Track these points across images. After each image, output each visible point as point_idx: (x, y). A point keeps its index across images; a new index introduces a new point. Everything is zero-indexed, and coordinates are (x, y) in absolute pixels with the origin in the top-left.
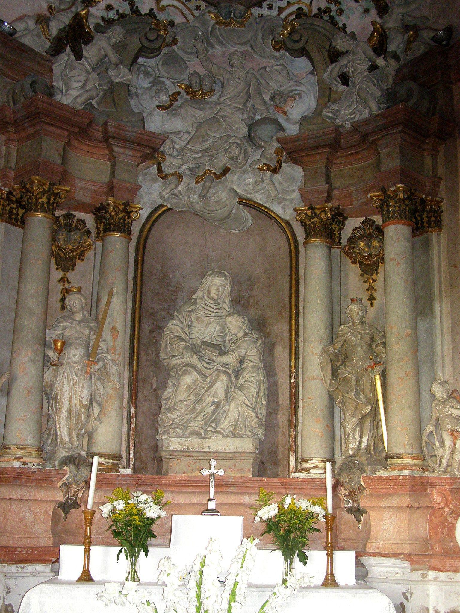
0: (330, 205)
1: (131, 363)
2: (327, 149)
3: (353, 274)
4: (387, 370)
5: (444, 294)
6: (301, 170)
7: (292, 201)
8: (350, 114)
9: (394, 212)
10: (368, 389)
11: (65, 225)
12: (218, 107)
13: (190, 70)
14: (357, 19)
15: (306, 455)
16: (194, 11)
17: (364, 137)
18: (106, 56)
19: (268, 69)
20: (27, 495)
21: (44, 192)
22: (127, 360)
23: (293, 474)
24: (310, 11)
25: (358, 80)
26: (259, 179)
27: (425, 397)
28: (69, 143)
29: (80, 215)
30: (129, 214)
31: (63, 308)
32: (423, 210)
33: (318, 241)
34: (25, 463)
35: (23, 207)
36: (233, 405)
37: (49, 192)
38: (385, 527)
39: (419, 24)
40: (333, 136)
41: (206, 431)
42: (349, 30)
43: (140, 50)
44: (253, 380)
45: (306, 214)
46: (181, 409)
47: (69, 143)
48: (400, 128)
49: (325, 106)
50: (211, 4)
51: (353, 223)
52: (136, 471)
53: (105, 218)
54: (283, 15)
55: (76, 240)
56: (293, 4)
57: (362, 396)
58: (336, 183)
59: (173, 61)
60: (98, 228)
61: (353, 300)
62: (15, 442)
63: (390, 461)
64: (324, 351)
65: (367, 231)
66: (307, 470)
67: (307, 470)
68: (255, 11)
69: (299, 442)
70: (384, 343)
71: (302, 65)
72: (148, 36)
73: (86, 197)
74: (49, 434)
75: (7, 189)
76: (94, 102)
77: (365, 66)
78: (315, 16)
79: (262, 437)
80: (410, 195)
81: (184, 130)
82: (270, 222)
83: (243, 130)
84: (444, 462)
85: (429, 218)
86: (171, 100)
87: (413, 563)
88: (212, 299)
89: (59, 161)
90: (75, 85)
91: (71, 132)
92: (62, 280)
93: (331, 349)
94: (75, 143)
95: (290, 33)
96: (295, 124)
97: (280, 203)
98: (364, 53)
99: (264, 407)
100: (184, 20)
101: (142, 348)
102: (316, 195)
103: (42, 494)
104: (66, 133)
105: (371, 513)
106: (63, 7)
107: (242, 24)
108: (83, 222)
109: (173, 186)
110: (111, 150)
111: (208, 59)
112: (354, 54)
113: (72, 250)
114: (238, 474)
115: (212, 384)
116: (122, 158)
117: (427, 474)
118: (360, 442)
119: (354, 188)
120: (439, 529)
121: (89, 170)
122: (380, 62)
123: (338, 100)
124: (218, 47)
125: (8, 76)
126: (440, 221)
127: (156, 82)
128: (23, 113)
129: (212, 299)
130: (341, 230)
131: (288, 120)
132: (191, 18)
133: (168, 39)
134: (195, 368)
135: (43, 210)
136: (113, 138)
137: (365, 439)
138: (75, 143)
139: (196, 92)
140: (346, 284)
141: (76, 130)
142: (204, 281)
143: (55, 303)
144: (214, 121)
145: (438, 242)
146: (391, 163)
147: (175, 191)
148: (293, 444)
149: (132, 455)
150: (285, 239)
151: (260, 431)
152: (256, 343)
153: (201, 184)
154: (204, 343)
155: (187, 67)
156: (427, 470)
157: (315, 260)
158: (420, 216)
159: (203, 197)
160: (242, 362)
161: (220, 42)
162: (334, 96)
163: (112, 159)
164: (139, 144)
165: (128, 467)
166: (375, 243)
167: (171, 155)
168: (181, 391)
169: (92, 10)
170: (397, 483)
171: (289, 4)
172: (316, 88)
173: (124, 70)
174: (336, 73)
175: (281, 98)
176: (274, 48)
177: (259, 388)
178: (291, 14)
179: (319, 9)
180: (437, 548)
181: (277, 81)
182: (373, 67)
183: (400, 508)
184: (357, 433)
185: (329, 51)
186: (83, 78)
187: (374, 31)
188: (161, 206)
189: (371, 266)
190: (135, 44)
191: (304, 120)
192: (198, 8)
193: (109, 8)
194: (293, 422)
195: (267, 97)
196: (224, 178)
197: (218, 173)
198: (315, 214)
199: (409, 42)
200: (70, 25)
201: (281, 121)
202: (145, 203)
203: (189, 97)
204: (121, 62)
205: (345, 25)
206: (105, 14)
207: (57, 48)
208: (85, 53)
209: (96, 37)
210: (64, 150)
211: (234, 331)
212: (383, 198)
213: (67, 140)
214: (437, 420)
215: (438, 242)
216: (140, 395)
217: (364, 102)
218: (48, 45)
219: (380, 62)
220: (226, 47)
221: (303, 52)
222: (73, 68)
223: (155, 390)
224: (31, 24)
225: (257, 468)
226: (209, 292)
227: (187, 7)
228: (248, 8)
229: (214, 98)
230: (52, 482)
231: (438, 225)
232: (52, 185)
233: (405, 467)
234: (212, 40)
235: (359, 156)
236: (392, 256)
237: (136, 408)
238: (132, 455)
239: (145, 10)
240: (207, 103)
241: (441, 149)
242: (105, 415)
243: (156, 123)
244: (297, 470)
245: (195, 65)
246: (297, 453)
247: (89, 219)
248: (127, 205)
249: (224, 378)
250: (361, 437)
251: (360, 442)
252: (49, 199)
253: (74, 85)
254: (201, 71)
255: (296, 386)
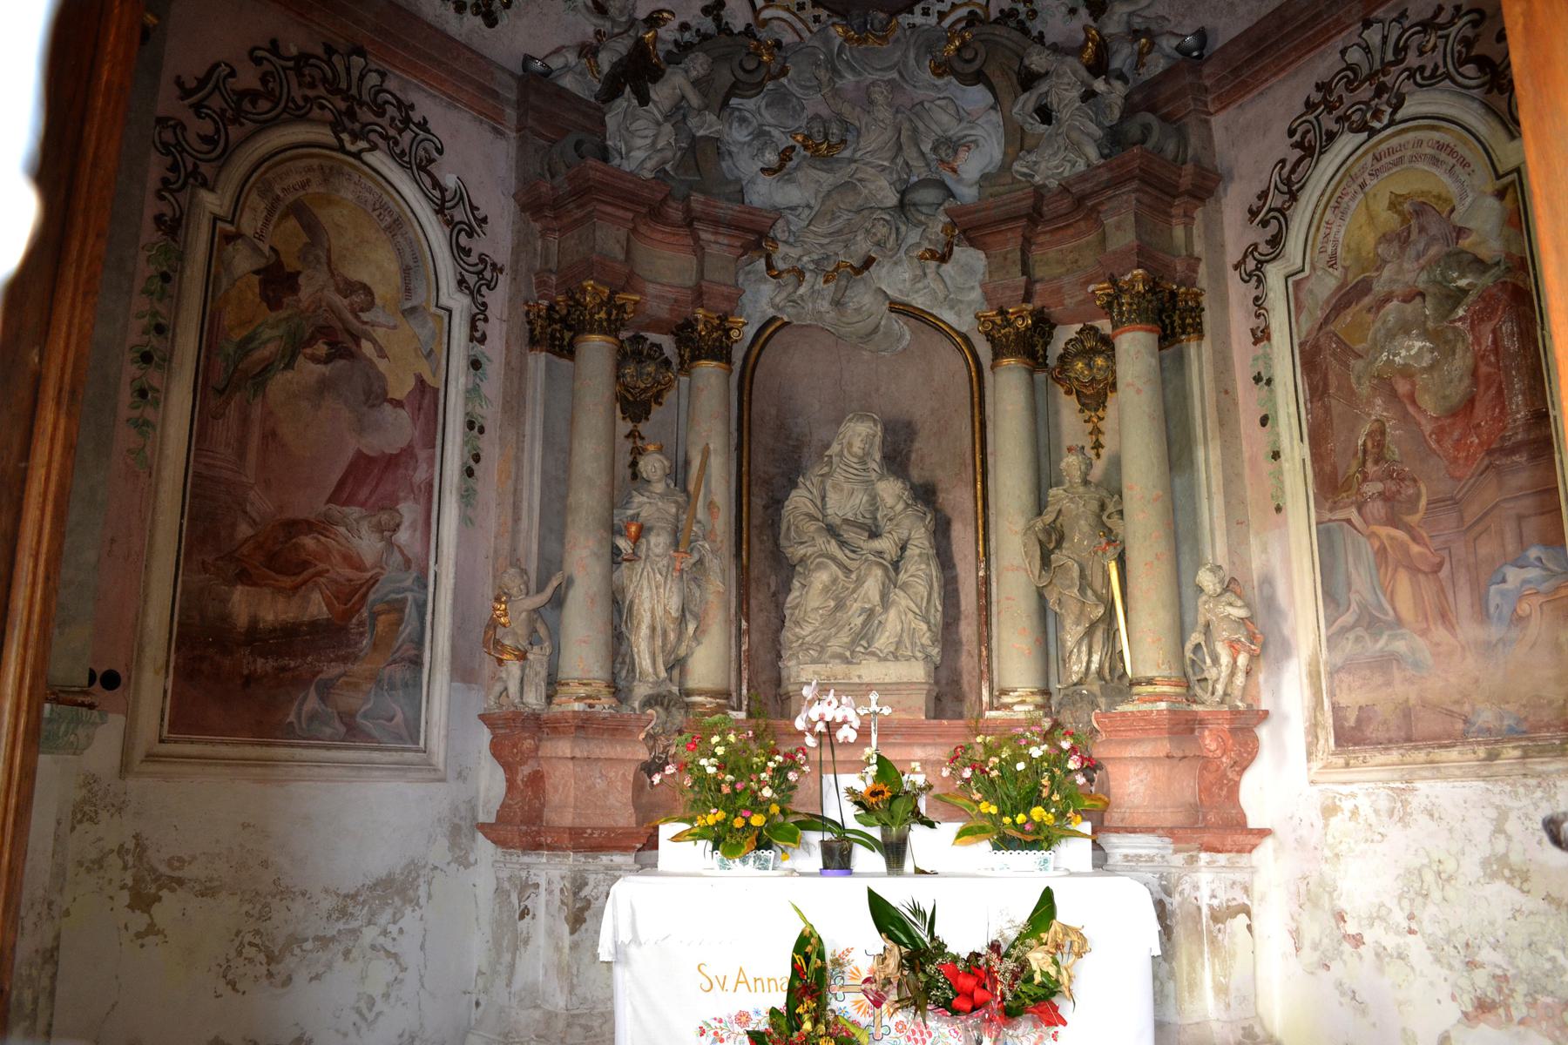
0: (1030, 307)
1: (738, 555)
2: (1023, 222)
3: (1068, 410)
4: (1127, 552)
5: (1209, 434)
6: (983, 256)
7: (970, 304)
8: (1057, 167)
9: (1130, 312)
10: (1098, 583)
11: (632, 353)
12: (854, 166)
13: (809, 112)
14: (1059, 19)
15: (1006, 685)
16: (811, 25)
17: (1080, 201)
18: (683, 97)
19: (927, 105)
20: (597, 753)
21: (601, 304)
22: (733, 550)
23: (988, 714)
24: (987, 14)
25: (1065, 115)
26: (919, 272)
27: (1188, 592)
28: (634, 230)
29: (653, 337)
30: (727, 332)
31: (635, 476)
32: (1174, 308)
33: (1012, 361)
34: (591, 706)
35: (570, 328)
36: (893, 613)
37: (609, 303)
38: (1132, 789)
39: (1154, 27)
40: (1030, 201)
41: (853, 652)
42: (1049, 39)
43: (734, 86)
44: (920, 573)
45: (993, 322)
46: (815, 620)
47: (634, 230)
48: (1135, 184)
49: (1017, 158)
50: (837, 13)
51: (1065, 334)
52: (750, 715)
53: (692, 339)
54: (946, 23)
55: (649, 374)
56: (961, 6)
57: (1089, 592)
58: (1039, 272)
59: (781, 100)
60: (682, 356)
61: (1070, 450)
62: (576, 674)
63: (1136, 689)
64: (1029, 529)
65: (1088, 345)
66: (1008, 707)
67: (1008, 707)
68: (904, 19)
69: (995, 665)
70: (1121, 513)
71: (977, 96)
72: (742, 63)
73: (662, 311)
74: (623, 662)
75: (546, 303)
76: (668, 167)
77: (1075, 94)
78: (996, 21)
79: (938, 659)
80: (1154, 286)
81: (803, 203)
82: (938, 337)
83: (892, 199)
84: (1220, 688)
85: (1183, 319)
86: (782, 160)
87: (1176, 840)
88: (854, 456)
89: (622, 257)
90: (639, 142)
91: (637, 213)
92: (630, 435)
93: (1039, 525)
94: (643, 229)
95: (958, 50)
96: (971, 186)
97: (952, 308)
98: (1074, 73)
99: (939, 615)
100: (797, 39)
101: (754, 532)
102: (1008, 293)
103: (617, 751)
104: (630, 215)
105: (1110, 768)
106: (616, 31)
107: (884, 39)
108: (659, 347)
109: (790, 288)
110: (697, 239)
111: (836, 93)
112: (1058, 76)
113: (645, 390)
114: (904, 716)
115: (860, 582)
116: (713, 250)
117: (1195, 707)
118: (1089, 662)
119: (1066, 280)
120: (1215, 789)
121: (666, 271)
122: (1099, 85)
123: (1037, 146)
124: (850, 77)
125: (541, 135)
126: (1200, 324)
127: (760, 133)
128: (566, 188)
129: (854, 456)
130: (1046, 344)
131: (960, 181)
132: (806, 34)
133: (775, 68)
134: (834, 559)
135: (602, 331)
136: (699, 219)
137: (1096, 658)
138: (643, 229)
139: (823, 145)
140: (1058, 426)
141: (644, 210)
142: (842, 429)
143: (623, 471)
144: (849, 186)
145: (1200, 356)
146: (1123, 237)
147: (795, 297)
148: (986, 670)
149: (744, 691)
150: (962, 362)
151: (935, 651)
152: (923, 519)
153: (832, 285)
154: (846, 521)
155: (803, 108)
156: (1195, 702)
157: (1009, 389)
158: (1169, 317)
159: (837, 303)
160: (903, 549)
161: (853, 69)
162: (1029, 142)
163: (699, 249)
164: (737, 228)
165: (740, 709)
166: (1100, 361)
167: (786, 242)
168: (811, 597)
169: (661, 32)
170: (1150, 722)
171: (954, 6)
172: (1001, 130)
173: (710, 117)
174: (1031, 106)
175: (951, 146)
176: (933, 73)
177: (931, 587)
178: (959, 20)
179: (1002, 11)
180: (1211, 817)
181: (944, 122)
182: (1089, 95)
183: (1155, 760)
184: (1084, 648)
185: (1019, 73)
186: (650, 133)
187: (1087, 39)
188: (773, 319)
189: (1095, 397)
190: (725, 77)
191: (985, 178)
192: (817, 19)
193: (684, 27)
194: (985, 639)
195: (926, 148)
196: (866, 273)
197: (855, 264)
198: (1008, 320)
199: (1141, 54)
200: (629, 55)
201: (949, 182)
202: (748, 317)
203: (808, 154)
204: (706, 107)
205: (1041, 33)
206: (678, 36)
207: (611, 90)
208: (653, 95)
209: (669, 70)
210: (628, 240)
211: (890, 501)
212: (1111, 291)
213: (631, 225)
214: (1208, 625)
215: (1200, 356)
216: (753, 602)
217: (1076, 147)
218: (598, 87)
219: (1099, 85)
220: (860, 74)
221: (979, 77)
222: (635, 118)
223: (774, 595)
224: (572, 58)
225: (932, 705)
226: (850, 445)
227: (801, 20)
228: (893, 14)
229: (847, 153)
230: (630, 733)
231: (1199, 331)
232: (613, 293)
233: (1159, 697)
234: (841, 67)
235: (1071, 231)
236: (1129, 379)
237: (748, 621)
238: (744, 691)
239: (738, 25)
240: (837, 160)
241: (1198, 214)
242: (704, 632)
243: (764, 193)
244: (991, 707)
245: (815, 104)
246: (991, 682)
247: (667, 343)
248: (723, 318)
249: (879, 572)
250: (1090, 654)
251: (1089, 662)
252: (609, 314)
253: (640, 141)
254: (825, 112)
255: (987, 581)
